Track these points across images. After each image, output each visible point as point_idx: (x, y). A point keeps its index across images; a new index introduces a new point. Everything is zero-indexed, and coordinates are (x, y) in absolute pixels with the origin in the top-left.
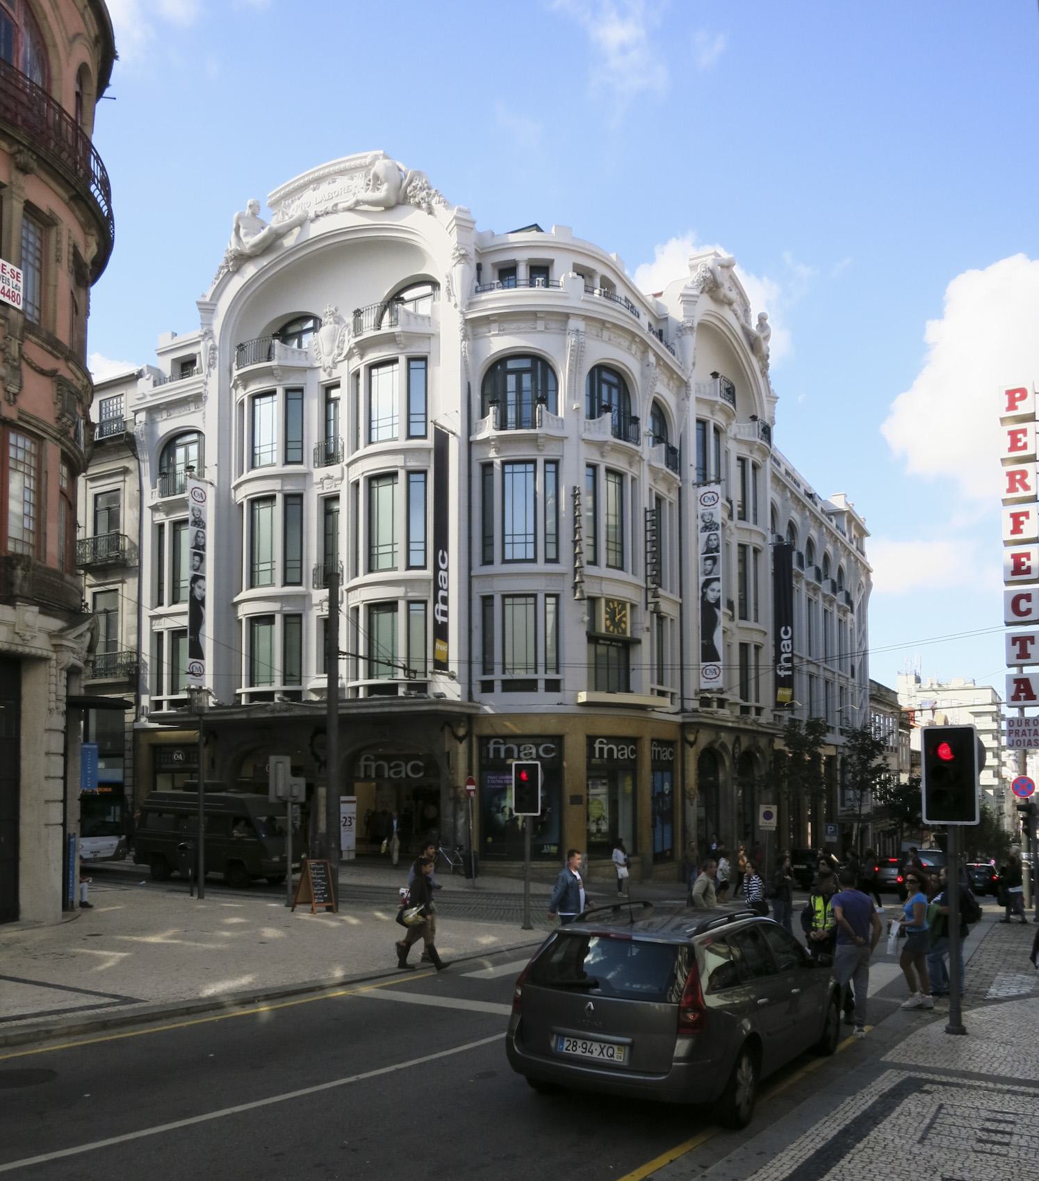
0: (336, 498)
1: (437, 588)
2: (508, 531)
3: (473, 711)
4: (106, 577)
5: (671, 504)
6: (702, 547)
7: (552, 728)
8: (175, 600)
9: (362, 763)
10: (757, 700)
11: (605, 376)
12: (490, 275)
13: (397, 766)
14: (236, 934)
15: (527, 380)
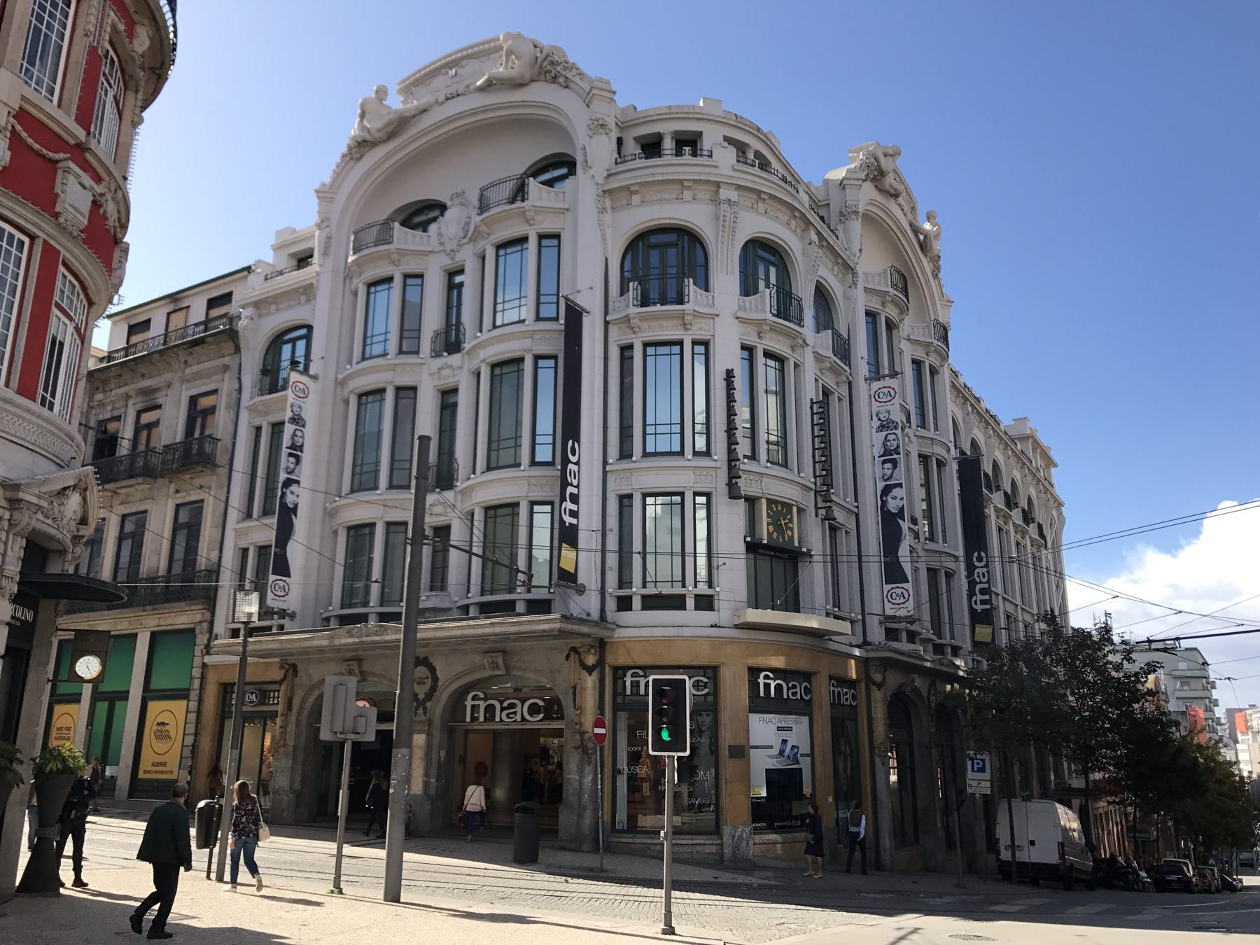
0: (455, 391)
2: (650, 420)
5: (840, 399)
6: (878, 450)
10: (953, 637)
12: (632, 148)
13: (512, 706)
14: (993, 908)
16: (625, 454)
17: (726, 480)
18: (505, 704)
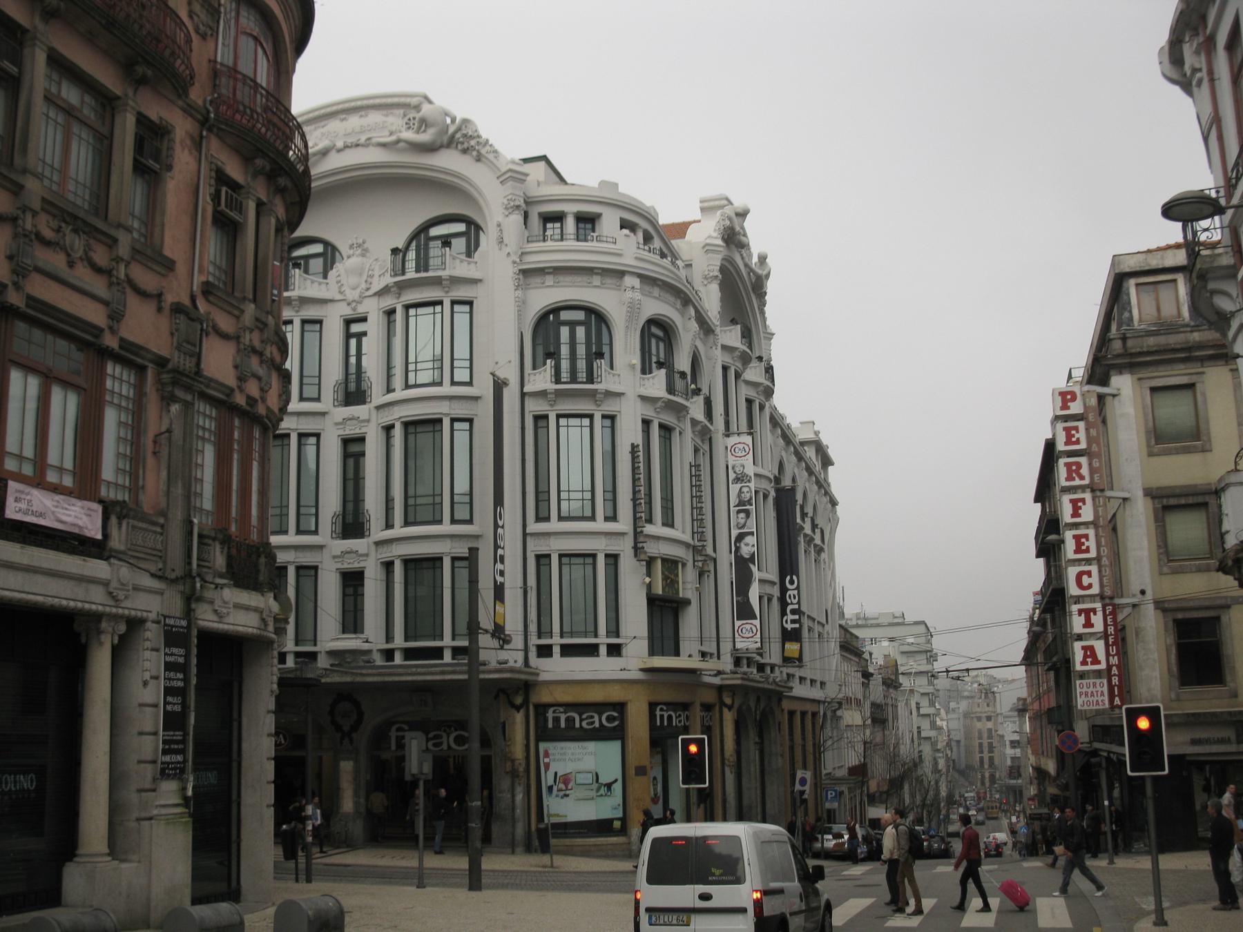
0: (362, 440)
3: (533, 678)
6: (734, 500)
7: (615, 695)
11: (654, 330)
12: (535, 221)
15: (581, 332)
17: (632, 544)
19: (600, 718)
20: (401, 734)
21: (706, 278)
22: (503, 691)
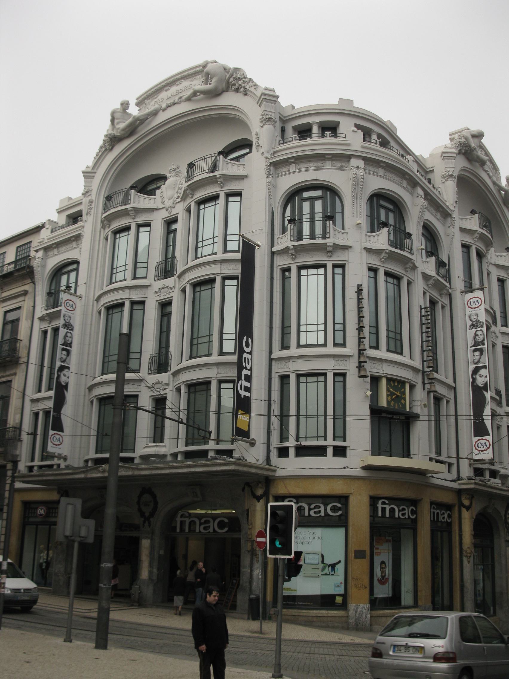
1: (240, 367)
2: (303, 321)
3: (270, 473)
4: (5, 371)
6: (470, 342)
7: (339, 488)
8: (50, 389)
9: (179, 519)
15: (318, 205)
16: (285, 346)
18: (203, 521)
19: (332, 509)
20: (183, 519)
21: (444, 178)
22: (248, 484)
